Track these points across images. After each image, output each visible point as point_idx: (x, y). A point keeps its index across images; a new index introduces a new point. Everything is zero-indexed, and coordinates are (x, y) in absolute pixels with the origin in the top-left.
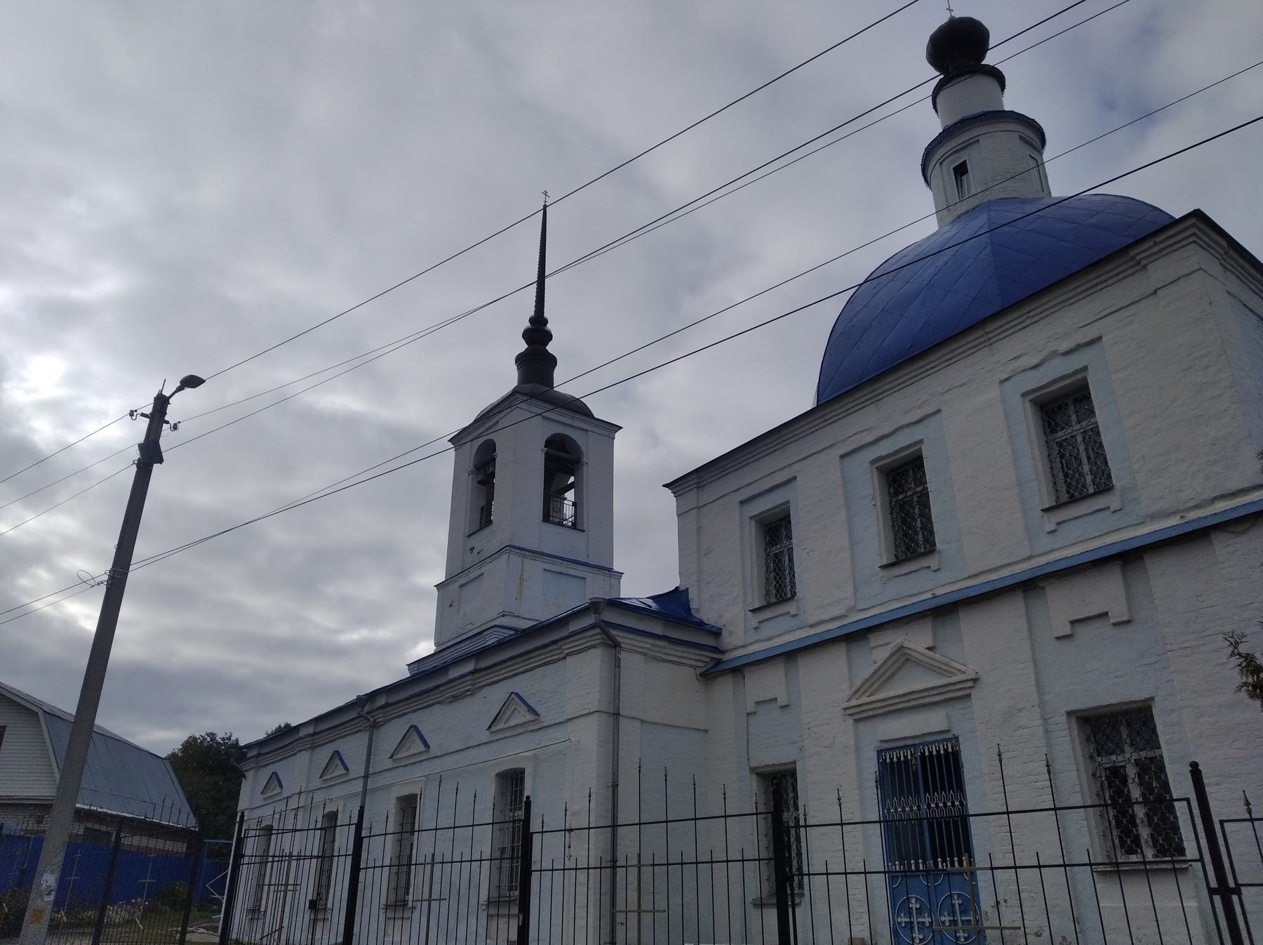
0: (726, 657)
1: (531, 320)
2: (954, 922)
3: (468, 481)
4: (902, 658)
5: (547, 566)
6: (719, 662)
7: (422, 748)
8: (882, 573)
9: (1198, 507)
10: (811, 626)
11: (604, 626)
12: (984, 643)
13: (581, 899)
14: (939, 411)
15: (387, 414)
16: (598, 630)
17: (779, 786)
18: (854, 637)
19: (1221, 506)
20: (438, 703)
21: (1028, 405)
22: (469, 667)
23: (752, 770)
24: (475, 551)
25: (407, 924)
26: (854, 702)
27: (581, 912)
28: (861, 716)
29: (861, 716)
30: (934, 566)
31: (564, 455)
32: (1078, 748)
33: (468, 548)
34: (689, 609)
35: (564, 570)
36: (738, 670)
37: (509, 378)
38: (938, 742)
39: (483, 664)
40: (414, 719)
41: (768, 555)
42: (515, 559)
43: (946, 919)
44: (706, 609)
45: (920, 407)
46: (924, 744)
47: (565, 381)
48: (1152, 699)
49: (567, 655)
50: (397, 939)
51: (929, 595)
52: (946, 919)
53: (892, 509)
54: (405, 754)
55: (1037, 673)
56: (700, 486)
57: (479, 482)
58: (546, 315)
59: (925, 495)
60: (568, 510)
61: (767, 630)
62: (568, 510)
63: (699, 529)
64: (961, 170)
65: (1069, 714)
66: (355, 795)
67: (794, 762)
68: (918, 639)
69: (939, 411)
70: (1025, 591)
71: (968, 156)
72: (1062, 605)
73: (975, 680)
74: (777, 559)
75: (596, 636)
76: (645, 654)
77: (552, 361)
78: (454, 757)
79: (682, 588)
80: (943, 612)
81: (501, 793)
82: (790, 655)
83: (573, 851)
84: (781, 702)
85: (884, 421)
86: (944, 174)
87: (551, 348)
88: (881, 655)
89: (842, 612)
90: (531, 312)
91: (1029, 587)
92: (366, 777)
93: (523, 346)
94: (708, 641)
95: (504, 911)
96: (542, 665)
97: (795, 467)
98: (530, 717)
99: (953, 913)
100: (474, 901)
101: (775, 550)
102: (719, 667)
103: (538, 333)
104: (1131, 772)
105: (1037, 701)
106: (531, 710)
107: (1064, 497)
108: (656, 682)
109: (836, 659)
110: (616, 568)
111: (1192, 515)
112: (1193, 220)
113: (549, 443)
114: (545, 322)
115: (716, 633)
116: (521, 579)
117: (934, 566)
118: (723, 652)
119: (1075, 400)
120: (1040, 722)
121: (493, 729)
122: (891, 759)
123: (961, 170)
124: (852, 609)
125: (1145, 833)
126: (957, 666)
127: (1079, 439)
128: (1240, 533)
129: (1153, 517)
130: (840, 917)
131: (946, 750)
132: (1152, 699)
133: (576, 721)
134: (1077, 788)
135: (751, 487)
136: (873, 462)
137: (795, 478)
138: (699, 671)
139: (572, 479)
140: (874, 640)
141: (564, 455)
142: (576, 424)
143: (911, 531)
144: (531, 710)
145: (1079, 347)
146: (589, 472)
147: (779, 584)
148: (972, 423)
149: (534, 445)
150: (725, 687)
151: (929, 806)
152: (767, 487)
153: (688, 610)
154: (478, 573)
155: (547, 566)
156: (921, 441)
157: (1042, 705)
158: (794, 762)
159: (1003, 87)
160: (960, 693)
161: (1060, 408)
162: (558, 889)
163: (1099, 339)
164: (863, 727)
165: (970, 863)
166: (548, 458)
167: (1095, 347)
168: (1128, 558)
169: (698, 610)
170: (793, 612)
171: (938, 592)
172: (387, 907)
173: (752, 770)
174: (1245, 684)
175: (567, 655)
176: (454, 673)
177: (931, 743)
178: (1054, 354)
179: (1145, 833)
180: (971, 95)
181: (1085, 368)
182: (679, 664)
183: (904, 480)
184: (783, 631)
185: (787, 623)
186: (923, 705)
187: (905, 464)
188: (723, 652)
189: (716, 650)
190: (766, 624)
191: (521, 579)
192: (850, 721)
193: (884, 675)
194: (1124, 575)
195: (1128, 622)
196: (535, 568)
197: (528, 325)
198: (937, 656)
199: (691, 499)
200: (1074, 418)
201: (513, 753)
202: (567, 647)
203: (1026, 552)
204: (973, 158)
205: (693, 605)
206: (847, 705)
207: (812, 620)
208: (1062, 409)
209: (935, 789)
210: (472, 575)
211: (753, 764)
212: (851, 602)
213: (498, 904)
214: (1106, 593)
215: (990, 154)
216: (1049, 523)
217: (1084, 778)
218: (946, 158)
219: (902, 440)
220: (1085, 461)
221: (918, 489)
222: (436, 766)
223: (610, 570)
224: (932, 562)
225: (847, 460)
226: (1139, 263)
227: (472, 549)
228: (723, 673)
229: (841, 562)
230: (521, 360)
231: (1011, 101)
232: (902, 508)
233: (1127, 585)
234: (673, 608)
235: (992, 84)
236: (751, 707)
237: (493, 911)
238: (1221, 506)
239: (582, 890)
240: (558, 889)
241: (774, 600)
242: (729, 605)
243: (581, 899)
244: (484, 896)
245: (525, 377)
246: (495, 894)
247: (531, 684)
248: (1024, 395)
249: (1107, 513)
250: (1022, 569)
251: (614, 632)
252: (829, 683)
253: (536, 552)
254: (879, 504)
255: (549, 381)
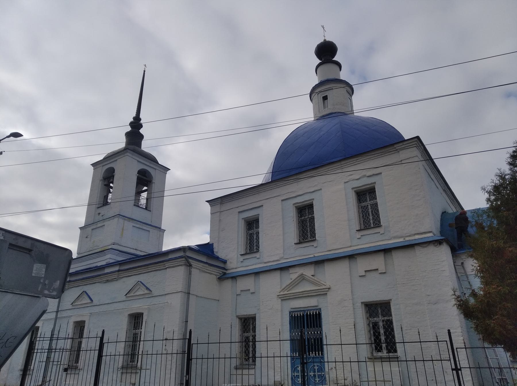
0: (228, 272)
1: (134, 118)
2: (315, 376)
3: (99, 184)
4: (302, 278)
5: (134, 225)
6: (225, 274)
7: (89, 301)
8: (295, 246)
9: (410, 236)
10: (265, 263)
11: (187, 258)
12: (333, 276)
13: (169, 367)
14: (321, 189)
15: (42, 142)
16: (184, 259)
17: (248, 323)
18: (284, 269)
19: (417, 237)
20: (99, 282)
21: (354, 192)
22: (117, 268)
23: (237, 316)
24: (101, 215)
25: (76, 376)
26: (282, 293)
27: (168, 372)
28: (284, 298)
29: (284, 298)
30: (315, 245)
31: (145, 178)
32: (364, 315)
33: (97, 213)
34: (213, 252)
35: (141, 227)
36: (234, 278)
37: (121, 143)
38: (313, 310)
39: (123, 268)
40: (86, 288)
41: (247, 234)
42: (121, 220)
43: (312, 374)
44: (220, 252)
45: (314, 186)
46: (308, 310)
47: (146, 146)
48: (391, 300)
49: (168, 268)
50: (71, 383)
51: (312, 256)
52: (312, 374)
53: (299, 222)
54: (80, 303)
55: (352, 287)
56: (221, 203)
57: (105, 185)
58: (141, 117)
59: (313, 218)
60: (143, 202)
61: (246, 263)
62: (143, 202)
63: (220, 220)
64: (325, 98)
65: (362, 303)
66: (51, 319)
67: (255, 314)
68: (308, 272)
69: (321, 189)
70: (349, 258)
71: (328, 93)
72: (363, 265)
73: (329, 288)
74: (251, 235)
75: (182, 261)
76: (200, 270)
77: (141, 137)
78: (106, 306)
79: (211, 243)
80: (319, 263)
81: (130, 322)
82: (257, 274)
83: (167, 348)
84: (251, 291)
85: (301, 189)
86: (318, 98)
87: (142, 131)
88: (294, 276)
89: (278, 258)
90: (134, 114)
91: (351, 257)
92: (57, 312)
93: (129, 129)
94: (222, 265)
95: (129, 371)
96: (154, 271)
97: (263, 202)
98: (146, 292)
99: (314, 372)
100: (116, 366)
101: (251, 232)
102: (225, 276)
103: (136, 124)
104: (381, 324)
105: (351, 298)
106: (147, 289)
107: (363, 227)
108: (203, 280)
109: (276, 277)
110: (162, 228)
111: (407, 239)
112: (416, 139)
113: (139, 172)
114: (140, 120)
115: (225, 262)
116: (123, 229)
117: (315, 245)
118: (226, 270)
119: (370, 193)
120: (352, 305)
121: (128, 295)
122: (295, 315)
123: (325, 98)
124: (282, 258)
125: (384, 345)
126: (322, 282)
127: (369, 207)
128: (424, 247)
129: (395, 238)
130: (271, 373)
131: (316, 313)
132: (391, 300)
133: (170, 295)
134: (363, 329)
135: (243, 207)
136: (294, 204)
137: (262, 206)
138: (218, 277)
139: (145, 188)
140: (291, 270)
141: (145, 178)
142: (151, 165)
143: (306, 230)
144: (147, 289)
145: (374, 175)
146: (155, 187)
147: (252, 245)
148: (332, 194)
149: (130, 173)
150: (228, 284)
151: (308, 333)
152: (250, 208)
153: (213, 252)
154: (102, 224)
155: (134, 225)
156: (313, 199)
157: (353, 299)
158: (255, 314)
159: (340, 70)
160: (323, 293)
161: (364, 194)
162: (159, 362)
163: (381, 173)
164: (285, 303)
165: (322, 354)
166: (138, 178)
167: (379, 176)
168: (386, 251)
169: (217, 252)
170: (258, 257)
171: (316, 255)
172: (123, 368)
173: (237, 316)
174: (456, 304)
175: (168, 268)
176: (107, 270)
177: (311, 310)
178: (364, 176)
179: (384, 345)
180: (329, 71)
181: (375, 183)
182: (211, 274)
183: (305, 213)
184: (253, 264)
185: (254, 261)
186: (309, 296)
187: (305, 206)
188: (226, 270)
189: (224, 269)
190: (246, 260)
191: (123, 229)
192: (280, 300)
193: (295, 284)
194: (384, 256)
195: (385, 273)
196: (129, 225)
197: (132, 120)
198: (315, 279)
199: (217, 208)
200: (368, 199)
201: (136, 307)
202: (167, 264)
203: (349, 244)
204: (330, 94)
205: (215, 250)
206: (279, 294)
207: (266, 261)
208: (365, 195)
209: (311, 327)
210: (99, 225)
211: (237, 314)
212: (283, 256)
213: (127, 368)
214: (378, 262)
215: (336, 94)
216: (358, 235)
217: (366, 325)
218: (320, 92)
219: (306, 198)
220: (371, 214)
221: (310, 216)
222: (96, 309)
223: (160, 228)
224: (315, 244)
225: (284, 202)
226: (395, 148)
227: (99, 214)
228: (228, 278)
229: (278, 238)
230: (128, 134)
231: (343, 75)
232: (302, 222)
233: (385, 261)
234: (206, 250)
235: (336, 67)
236: (238, 292)
237: (125, 371)
238: (417, 237)
239: (169, 363)
240: (159, 362)
241: (248, 251)
242: (231, 251)
243: (169, 367)
244: (120, 365)
245: (128, 143)
246: (125, 364)
247: (149, 278)
248: (353, 189)
249: (379, 234)
250: (348, 250)
251: (190, 260)
252: (272, 285)
253: (130, 218)
254: (295, 220)
255: (140, 145)
